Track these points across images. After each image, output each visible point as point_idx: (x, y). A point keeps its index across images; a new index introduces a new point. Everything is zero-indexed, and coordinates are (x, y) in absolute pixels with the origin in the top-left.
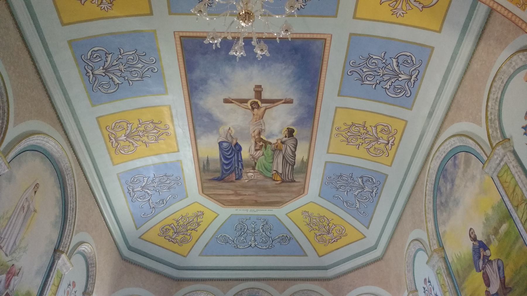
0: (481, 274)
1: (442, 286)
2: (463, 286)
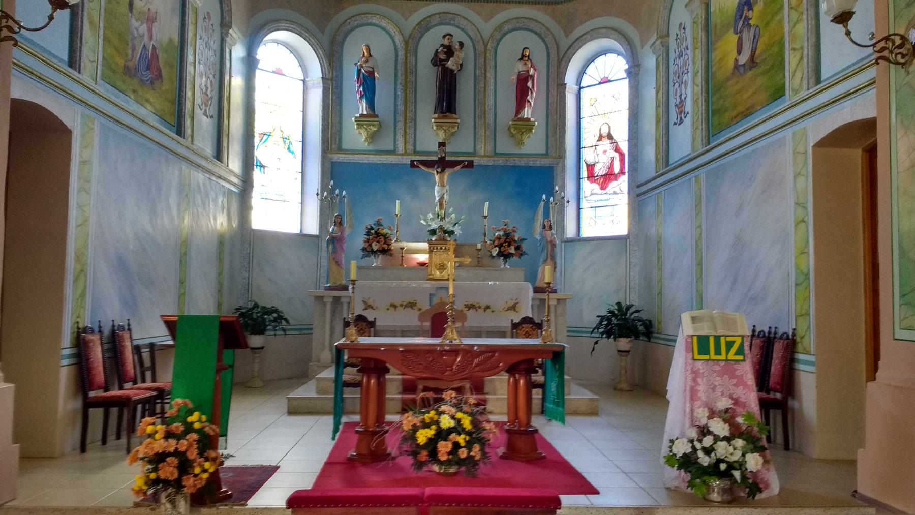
0: (736, 37)
1: (694, 39)
2: (716, 46)
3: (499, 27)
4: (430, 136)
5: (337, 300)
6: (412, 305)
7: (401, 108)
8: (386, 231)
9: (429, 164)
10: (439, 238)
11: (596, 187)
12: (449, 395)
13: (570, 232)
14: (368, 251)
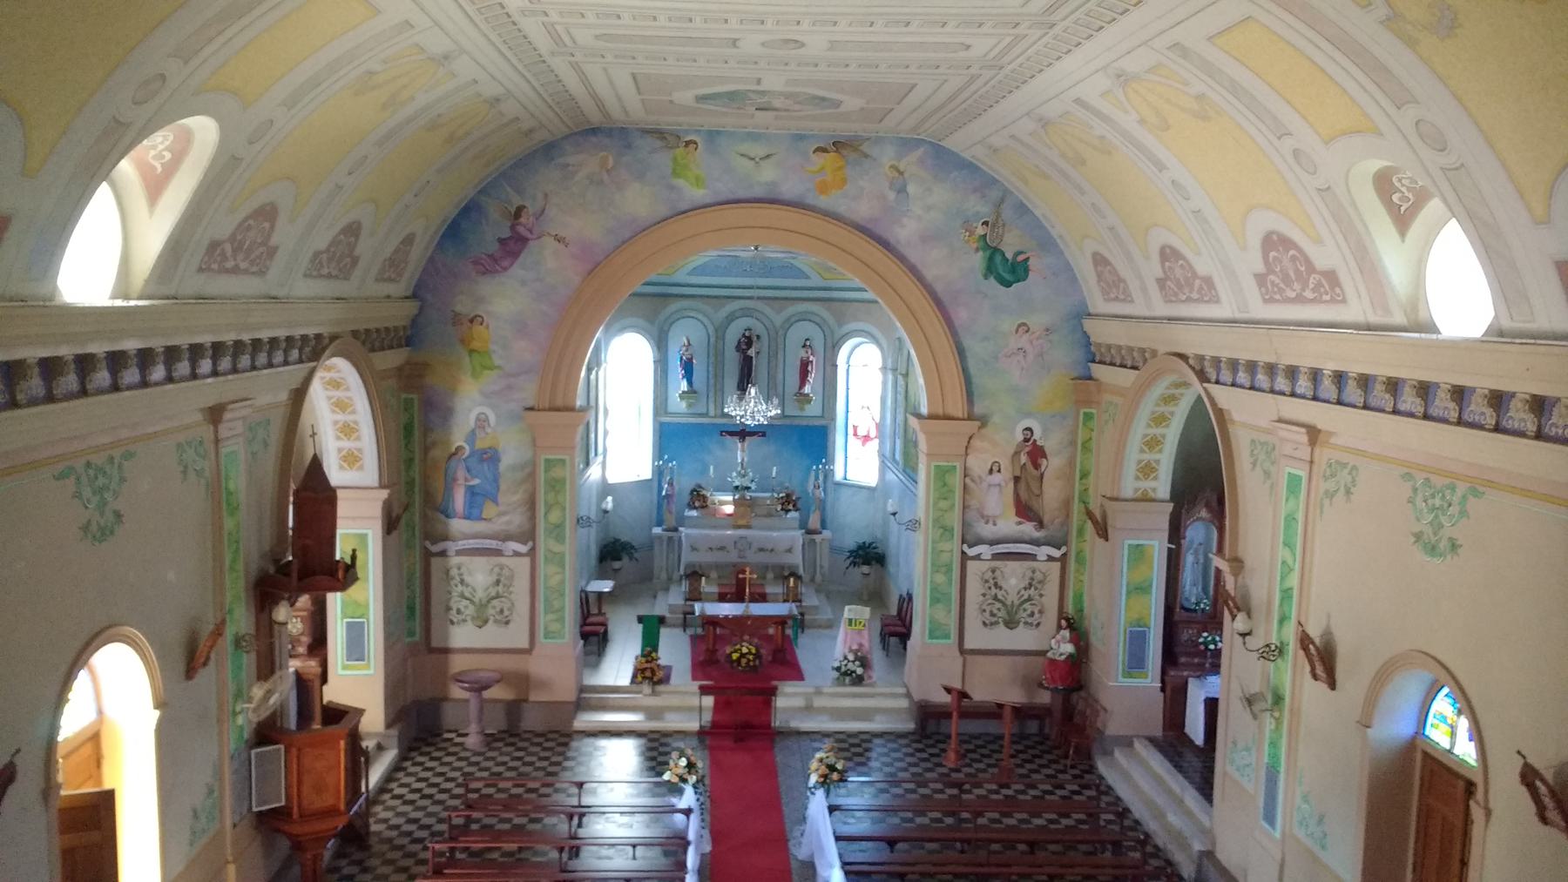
7: (712, 381)
11: (859, 442)
12: (746, 637)
13: (839, 476)
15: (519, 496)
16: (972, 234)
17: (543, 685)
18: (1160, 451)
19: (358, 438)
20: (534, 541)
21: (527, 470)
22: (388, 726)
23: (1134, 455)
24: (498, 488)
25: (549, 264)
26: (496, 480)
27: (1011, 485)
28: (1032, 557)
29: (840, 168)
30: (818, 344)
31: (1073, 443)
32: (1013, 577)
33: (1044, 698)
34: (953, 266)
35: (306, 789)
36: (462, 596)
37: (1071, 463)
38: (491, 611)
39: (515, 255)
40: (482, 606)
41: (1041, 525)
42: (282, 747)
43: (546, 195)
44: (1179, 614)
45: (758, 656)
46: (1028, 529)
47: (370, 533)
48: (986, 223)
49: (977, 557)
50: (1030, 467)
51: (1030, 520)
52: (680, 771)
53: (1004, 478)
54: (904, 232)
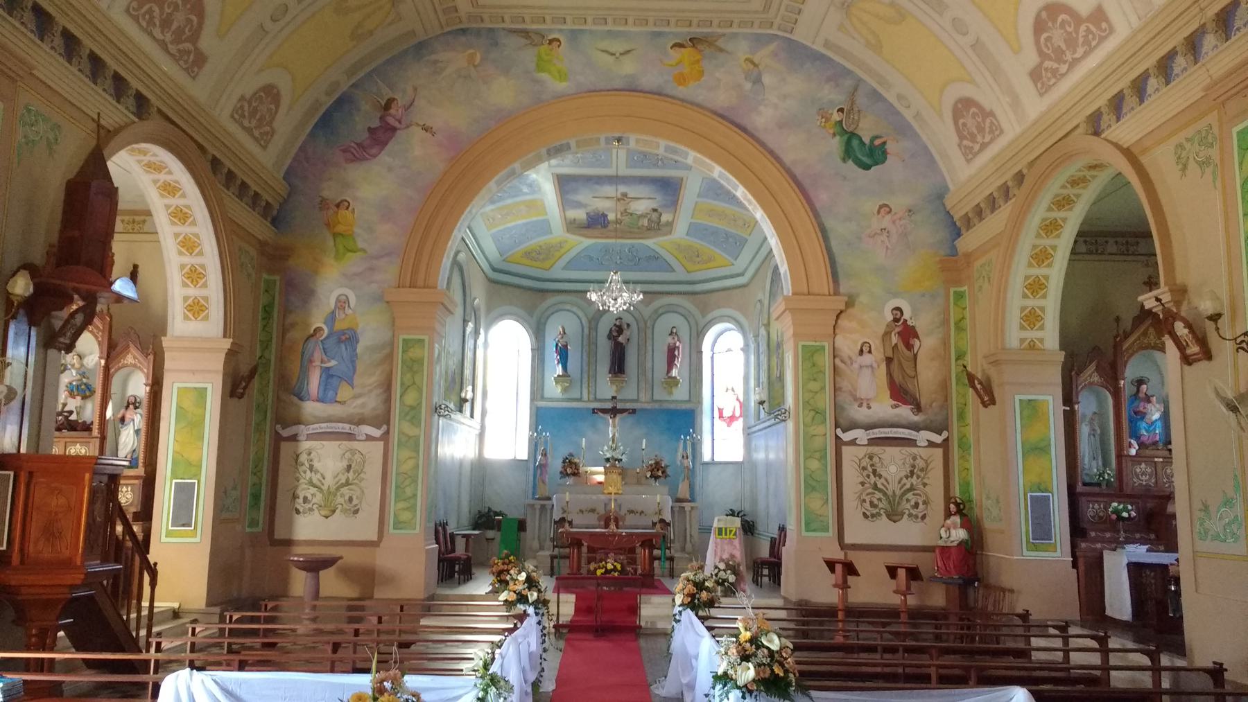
3: (656, 311)
4: (606, 388)
5: (543, 507)
6: (593, 511)
7: (585, 368)
8: (576, 460)
9: (604, 411)
10: (611, 464)
11: (724, 424)
13: (707, 457)
14: (564, 474)
15: (375, 378)
16: (827, 120)
17: (390, 580)
18: (1044, 297)
19: (205, 285)
20: (388, 425)
21: (386, 352)
22: (209, 604)
23: (1016, 302)
24: (355, 370)
25: (415, 151)
26: (353, 359)
27: (883, 366)
28: (911, 442)
29: (698, 61)
30: (684, 332)
31: (945, 322)
32: (893, 463)
33: (937, 598)
34: (815, 151)
35: (34, 531)
36: (311, 483)
37: (945, 343)
38: (340, 500)
39: (384, 144)
40: (330, 494)
41: (918, 408)
42: (12, 474)
43: (415, 89)
44: (1080, 488)
45: (623, 571)
46: (905, 412)
47: (209, 386)
48: (841, 110)
49: (853, 442)
50: (901, 346)
51: (905, 403)
52: (519, 587)
53: (876, 357)
54: (762, 119)
